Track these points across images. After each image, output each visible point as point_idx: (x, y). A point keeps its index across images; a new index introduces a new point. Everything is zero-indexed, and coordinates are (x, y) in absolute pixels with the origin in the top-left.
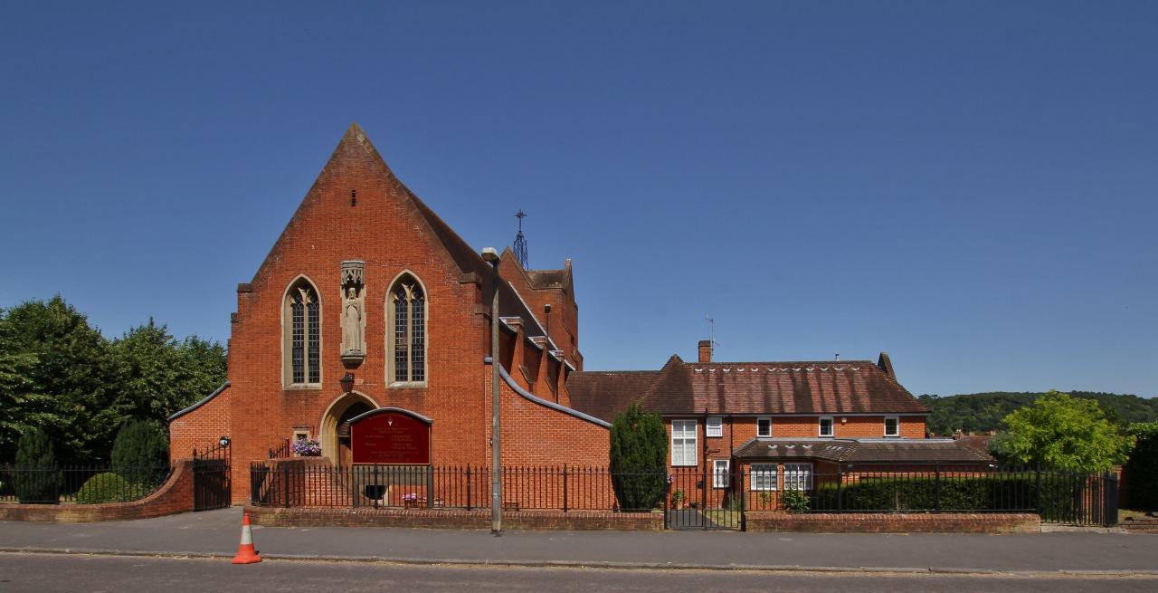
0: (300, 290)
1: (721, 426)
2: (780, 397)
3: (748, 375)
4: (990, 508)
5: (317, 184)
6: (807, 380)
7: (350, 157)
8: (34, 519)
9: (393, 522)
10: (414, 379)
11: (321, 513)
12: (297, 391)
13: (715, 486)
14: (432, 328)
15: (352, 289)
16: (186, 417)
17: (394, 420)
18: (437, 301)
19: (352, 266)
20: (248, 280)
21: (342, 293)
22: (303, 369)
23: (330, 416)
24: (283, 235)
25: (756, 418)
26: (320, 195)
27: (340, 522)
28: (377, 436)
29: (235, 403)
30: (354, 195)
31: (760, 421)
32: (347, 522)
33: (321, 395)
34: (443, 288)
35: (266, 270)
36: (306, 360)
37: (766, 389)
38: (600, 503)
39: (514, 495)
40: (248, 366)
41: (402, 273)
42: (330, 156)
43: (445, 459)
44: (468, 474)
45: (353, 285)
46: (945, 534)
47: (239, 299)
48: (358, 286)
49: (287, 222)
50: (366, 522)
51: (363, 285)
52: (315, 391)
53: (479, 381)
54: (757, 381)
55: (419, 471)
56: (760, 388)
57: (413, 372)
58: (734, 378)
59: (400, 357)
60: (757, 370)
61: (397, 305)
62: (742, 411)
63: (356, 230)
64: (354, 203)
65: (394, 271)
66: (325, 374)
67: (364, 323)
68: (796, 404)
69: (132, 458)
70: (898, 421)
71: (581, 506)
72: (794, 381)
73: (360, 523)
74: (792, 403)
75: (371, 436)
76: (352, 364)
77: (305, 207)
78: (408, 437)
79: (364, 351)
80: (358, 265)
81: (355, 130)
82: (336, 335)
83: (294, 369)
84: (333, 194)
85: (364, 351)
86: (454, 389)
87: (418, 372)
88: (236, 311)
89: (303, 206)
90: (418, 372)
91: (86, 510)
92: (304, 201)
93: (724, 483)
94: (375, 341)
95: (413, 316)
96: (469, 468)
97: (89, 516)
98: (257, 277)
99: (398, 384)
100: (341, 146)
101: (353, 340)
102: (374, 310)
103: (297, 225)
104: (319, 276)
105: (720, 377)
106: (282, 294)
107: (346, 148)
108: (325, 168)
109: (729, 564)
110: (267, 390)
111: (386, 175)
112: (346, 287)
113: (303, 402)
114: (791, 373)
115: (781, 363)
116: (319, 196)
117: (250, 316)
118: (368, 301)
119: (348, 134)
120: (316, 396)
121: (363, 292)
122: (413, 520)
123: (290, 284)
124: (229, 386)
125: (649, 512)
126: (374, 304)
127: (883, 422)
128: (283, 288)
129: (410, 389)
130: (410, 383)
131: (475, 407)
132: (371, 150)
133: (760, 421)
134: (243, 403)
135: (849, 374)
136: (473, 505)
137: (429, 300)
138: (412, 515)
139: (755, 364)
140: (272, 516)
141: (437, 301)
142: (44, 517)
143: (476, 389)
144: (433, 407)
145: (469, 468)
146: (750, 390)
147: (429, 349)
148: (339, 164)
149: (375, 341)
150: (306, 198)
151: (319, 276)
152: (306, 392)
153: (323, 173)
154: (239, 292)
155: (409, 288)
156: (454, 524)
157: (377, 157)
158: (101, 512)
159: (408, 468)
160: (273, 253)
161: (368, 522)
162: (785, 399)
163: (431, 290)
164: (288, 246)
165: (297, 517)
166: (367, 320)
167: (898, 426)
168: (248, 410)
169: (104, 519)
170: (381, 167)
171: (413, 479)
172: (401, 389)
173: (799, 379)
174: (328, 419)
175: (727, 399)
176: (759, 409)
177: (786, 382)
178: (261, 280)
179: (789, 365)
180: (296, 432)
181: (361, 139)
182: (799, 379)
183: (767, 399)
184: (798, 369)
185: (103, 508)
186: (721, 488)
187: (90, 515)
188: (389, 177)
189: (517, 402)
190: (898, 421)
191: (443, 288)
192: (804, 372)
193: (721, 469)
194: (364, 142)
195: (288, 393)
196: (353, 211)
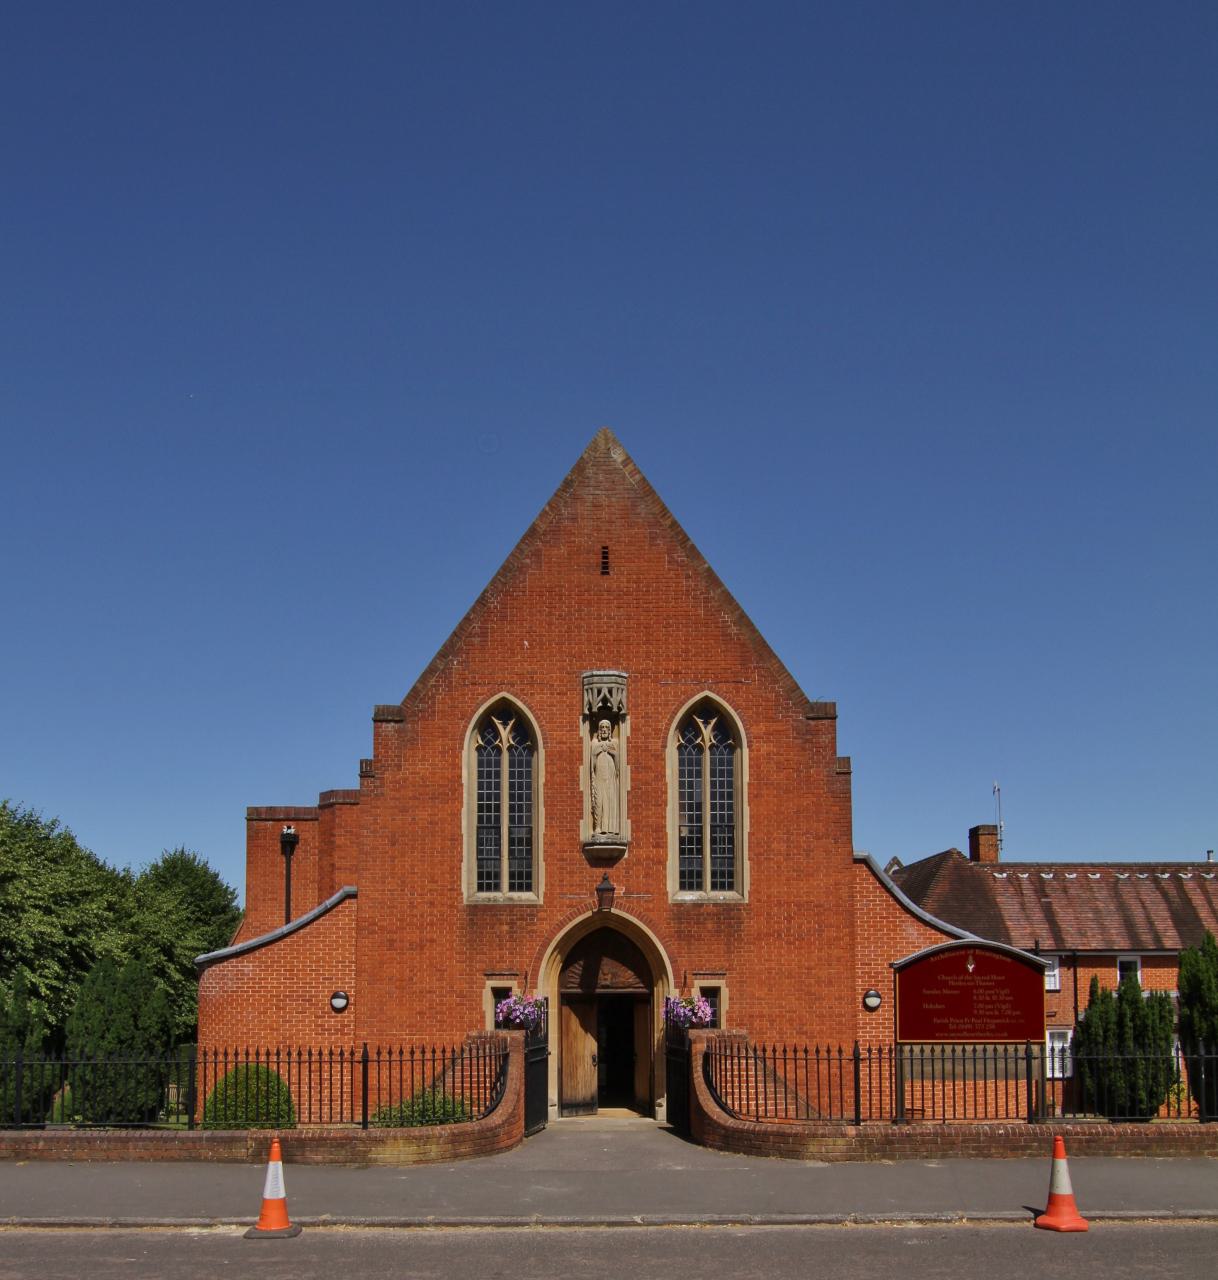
0: (496, 721)
1: (1057, 972)
2: (1150, 923)
3: (1085, 883)
4: (96, 1121)
5: (532, 532)
6: (1186, 894)
7: (597, 487)
8: (320, 1158)
9: (1076, 1145)
10: (714, 886)
11: (936, 1134)
12: (493, 907)
13: (1049, 1075)
14: (756, 796)
15: (605, 723)
16: (257, 954)
17: (978, 961)
18: (764, 748)
19: (610, 680)
20: (395, 698)
21: (584, 729)
22: (500, 866)
23: (555, 953)
24: (467, 619)
25: (1116, 957)
26: (539, 550)
27: (974, 1149)
28: (946, 992)
29: (363, 927)
30: (605, 555)
31: (1121, 963)
32: (989, 1148)
33: (544, 915)
34: (775, 727)
35: (432, 682)
36: (508, 852)
37: (1122, 908)
38: (991, 1109)
39: (980, 1092)
40: (393, 858)
41: (697, 697)
42: (558, 484)
43: (781, 1032)
44: (365, 1061)
45: (604, 715)
46: (710, 1150)
47: (377, 735)
48: (616, 719)
49: (477, 595)
50: (1024, 1148)
51: (624, 716)
52: (529, 906)
53: (844, 892)
54: (1102, 894)
55: (979, 1054)
56: (1112, 907)
57: (512, 876)
58: (1065, 890)
59: (690, 846)
60: (1098, 876)
61: (480, 754)
62: (1094, 946)
63: (609, 618)
64: (605, 569)
65: (684, 693)
66: (549, 875)
67: (627, 785)
68: (1181, 934)
69: (124, 1035)
70: (1139, 964)
71: (1002, 1113)
72: (1165, 895)
73: (1014, 1149)
74: (1172, 932)
75: (935, 992)
76: (603, 857)
77: (509, 572)
78: (1007, 991)
79: (626, 834)
80: (620, 680)
81: (607, 440)
82: (568, 802)
83: (480, 866)
84: (563, 550)
85: (626, 834)
86: (799, 905)
87: (722, 874)
88: (369, 755)
89: (505, 570)
90: (722, 874)
91: (427, 1139)
92: (508, 561)
93: (1063, 1069)
94: (648, 817)
95: (713, 774)
96: (365, 1054)
97: (434, 1150)
98: (414, 694)
99: (689, 896)
100: (580, 468)
101: (608, 814)
102: (645, 762)
103: (494, 603)
104: (537, 697)
105: (1040, 888)
106: (466, 727)
107: (590, 472)
108: (549, 504)
109: (319, 1214)
110: (432, 904)
111: (668, 522)
112: (593, 719)
113: (506, 928)
114: (1156, 881)
115: (1136, 865)
116: (537, 554)
117: (399, 767)
118: (633, 746)
119: (594, 447)
120: (532, 915)
121: (625, 728)
122: (1112, 1142)
123: (481, 710)
124: (353, 896)
125: (1147, 1121)
126: (647, 749)
127: (1115, 967)
128: (467, 717)
129: (715, 905)
130: (709, 895)
131: (838, 939)
132: (637, 477)
133: (1121, 963)
134: (382, 928)
135: (1115, 887)
136: (864, 1113)
137: (749, 747)
138: (1111, 1134)
139: (1092, 865)
140: (840, 1141)
141: (764, 748)
142: (342, 1154)
143: (838, 906)
144: (759, 937)
145: (365, 1054)
146: (1096, 911)
147: (751, 834)
148: (576, 498)
149: (648, 817)
150: (512, 555)
151: (537, 697)
152: (511, 907)
153: (544, 514)
154: (375, 721)
155: (505, 724)
156: (1191, 1148)
157: (647, 491)
158: (453, 1142)
159: (969, 1048)
160: (447, 651)
161: (1030, 1148)
162: (1160, 926)
163: (754, 730)
164: (477, 640)
165: (891, 1143)
166: (632, 780)
167: (1139, 973)
168: (392, 941)
169: (456, 1156)
170: (656, 510)
171: (1011, 1066)
172: (697, 905)
173: (1173, 892)
174: (550, 965)
175: (1063, 925)
176: (1121, 942)
177: (1151, 896)
178: (422, 701)
179: (1151, 869)
180: (491, 983)
181: (618, 456)
182: (1173, 892)
183: (1129, 925)
184: (1167, 876)
185: (453, 1134)
186: (1058, 1079)
187: (434, 1148)
188: (670, 527)
189: (911, 930)
190: (1139, 964)
191: (775, 727)
192: (1178, 882)
193: (1058, 1045)
194: (625, 463)
195: (475, 909)
196: (605, 582)
